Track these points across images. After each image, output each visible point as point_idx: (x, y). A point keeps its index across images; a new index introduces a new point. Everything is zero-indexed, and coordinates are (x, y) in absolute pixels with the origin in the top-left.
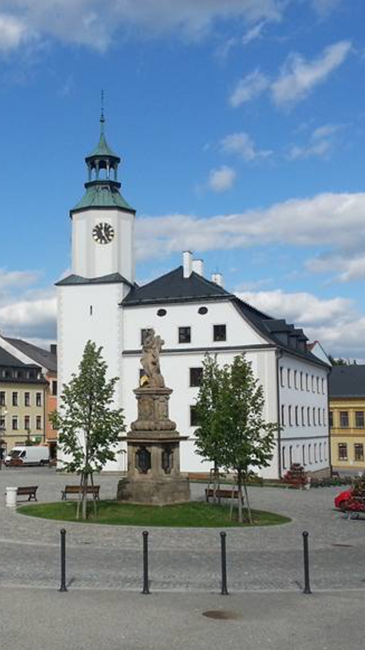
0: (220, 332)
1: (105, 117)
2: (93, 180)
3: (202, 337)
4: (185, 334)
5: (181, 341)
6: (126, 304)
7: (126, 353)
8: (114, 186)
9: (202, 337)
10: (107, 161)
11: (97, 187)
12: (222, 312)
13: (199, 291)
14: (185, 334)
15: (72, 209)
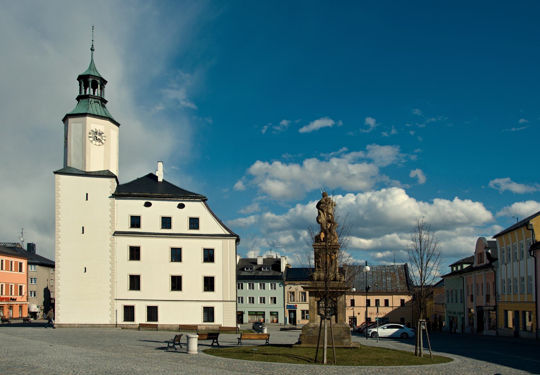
0: (194, 223)
1: (95, 47)
2: (83, 94)
3: (180, 225)
4: (166, 222)
7: (117, 233)
9: (180, 225)
14: (166, 222)
15: (69, 112)
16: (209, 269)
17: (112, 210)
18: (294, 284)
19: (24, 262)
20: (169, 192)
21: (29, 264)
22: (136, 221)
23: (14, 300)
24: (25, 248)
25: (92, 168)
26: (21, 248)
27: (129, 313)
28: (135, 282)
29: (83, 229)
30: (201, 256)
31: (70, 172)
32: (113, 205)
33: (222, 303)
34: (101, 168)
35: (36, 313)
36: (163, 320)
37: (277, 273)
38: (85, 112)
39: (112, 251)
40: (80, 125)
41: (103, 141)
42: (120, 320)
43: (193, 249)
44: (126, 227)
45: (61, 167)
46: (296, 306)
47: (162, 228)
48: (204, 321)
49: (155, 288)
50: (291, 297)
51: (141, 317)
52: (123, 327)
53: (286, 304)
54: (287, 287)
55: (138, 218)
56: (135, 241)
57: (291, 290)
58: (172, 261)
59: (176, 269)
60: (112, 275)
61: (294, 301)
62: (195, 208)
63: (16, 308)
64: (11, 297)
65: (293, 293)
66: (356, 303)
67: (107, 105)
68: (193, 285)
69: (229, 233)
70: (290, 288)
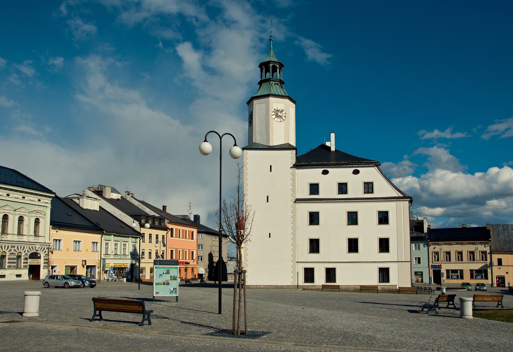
0: (369, 187)
3: (355, 189)
4: (343, 188)
5: (311, 193)
6: (298, 165)
7: (298, 201)
9: (355, 189)
10: (278, 66)
14: (343, 188)
16: (384, 231)
17: (293, 180)
18: (438, 244)
19: (195, 231)
20: (342, 159)
21: (199, 232)
22: (314, 188)
23: (188, 263)
24: (192, 219)
25: (274, 142)
26: (189, 219)
27: (309, 275)
28: (314, 246)
29: (268, 198)
30: (375, 218)
31: (256, 147)
32: (293, 175)
33: (396, 264)
34: (283, 142)
35: (203, 274)
36: (340, 280)
37: (420, 234)
38: (268, 93)
39: (294, 217)
40: (263, 106)
41: (284, 118)
42: (301, 282)
43: (368, 213)
44: (306, 195)
45: (246, 145)
46: (441, 265)
47: (339, 194)
48: (380, 282)
49: (334, 250)
50: (435, 257)
51: (320, 279)
52: (304, 289)
53: (431, 264)
54: (431, 248)
55: (317, 185)
56: (314, 207)
57: (436, 250)
58: (348, 224)
59: (353, 232)
60: (294, 239)
61: (438, 260)
62: (369, 173)
63: (189, 271)
64: (184, 261)
65: (437, 253)
66: (503, 263)
68: (369, 246)
69: (402, 196)
70: (434, 248)
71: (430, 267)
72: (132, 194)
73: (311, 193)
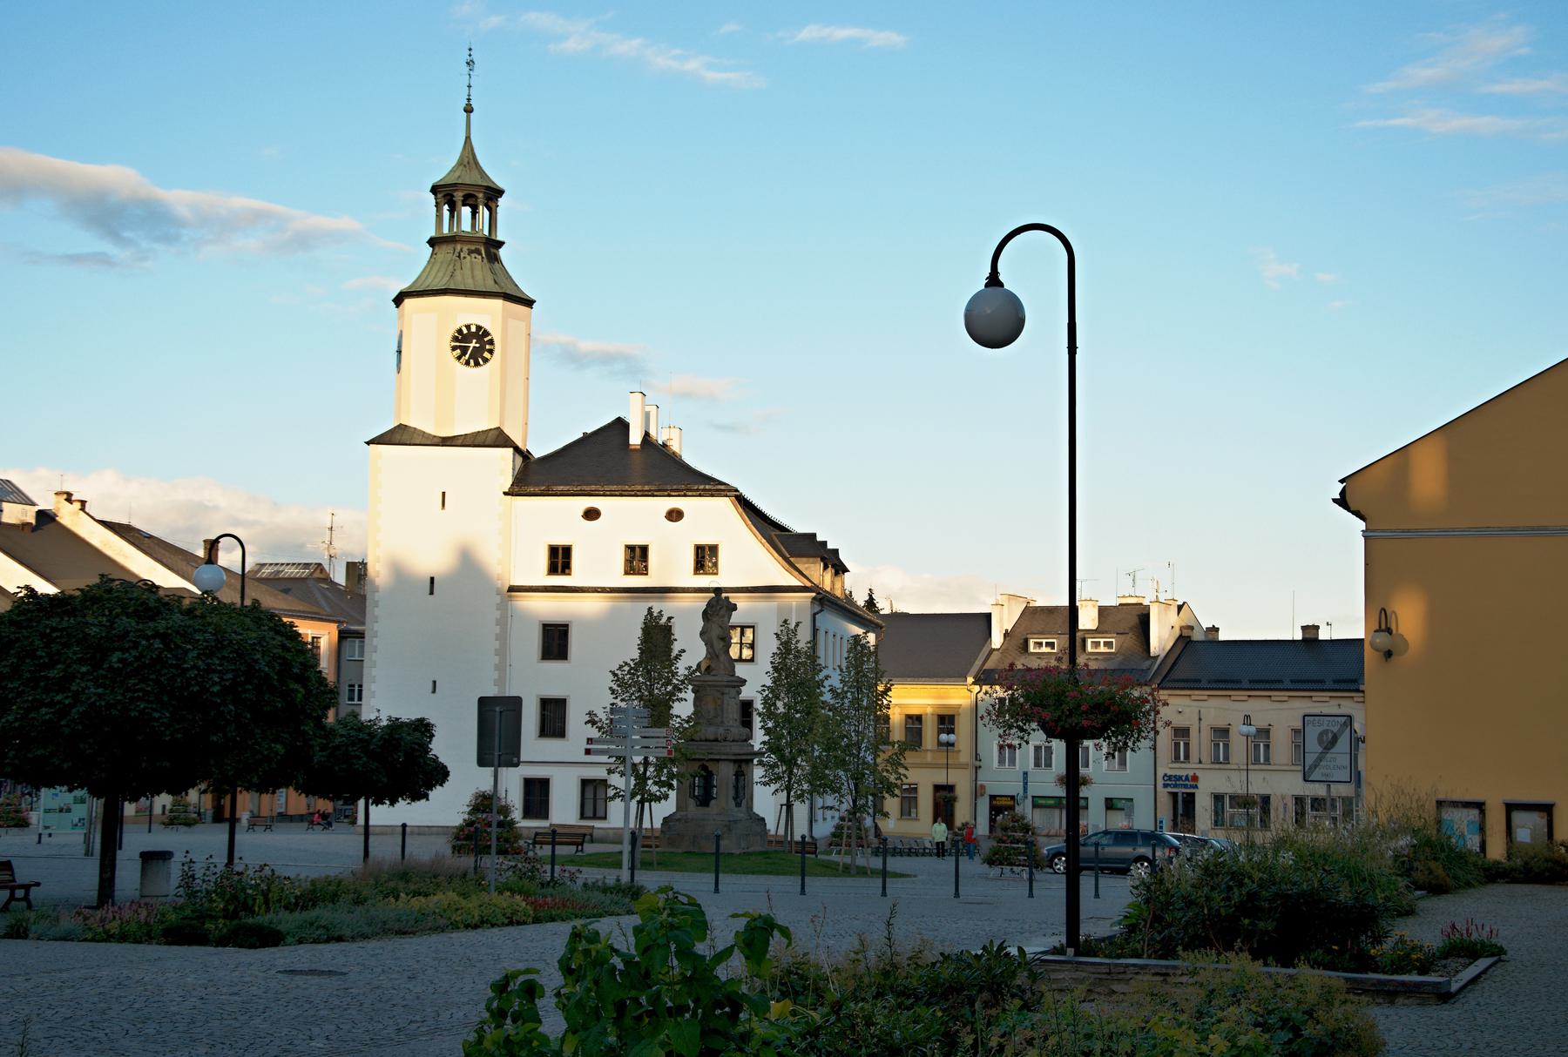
0: (705, 557)
2: (446, 231)
8: (492, 246)
11: (459, 247)
12: (711, 519)
13: (663, 472)
46: (1195, 778)
47: (626, 573)
55: (567, 551)
67: (502, 252)
71: (1160, 782)
72: (83, 503)
73: (553, 570)
